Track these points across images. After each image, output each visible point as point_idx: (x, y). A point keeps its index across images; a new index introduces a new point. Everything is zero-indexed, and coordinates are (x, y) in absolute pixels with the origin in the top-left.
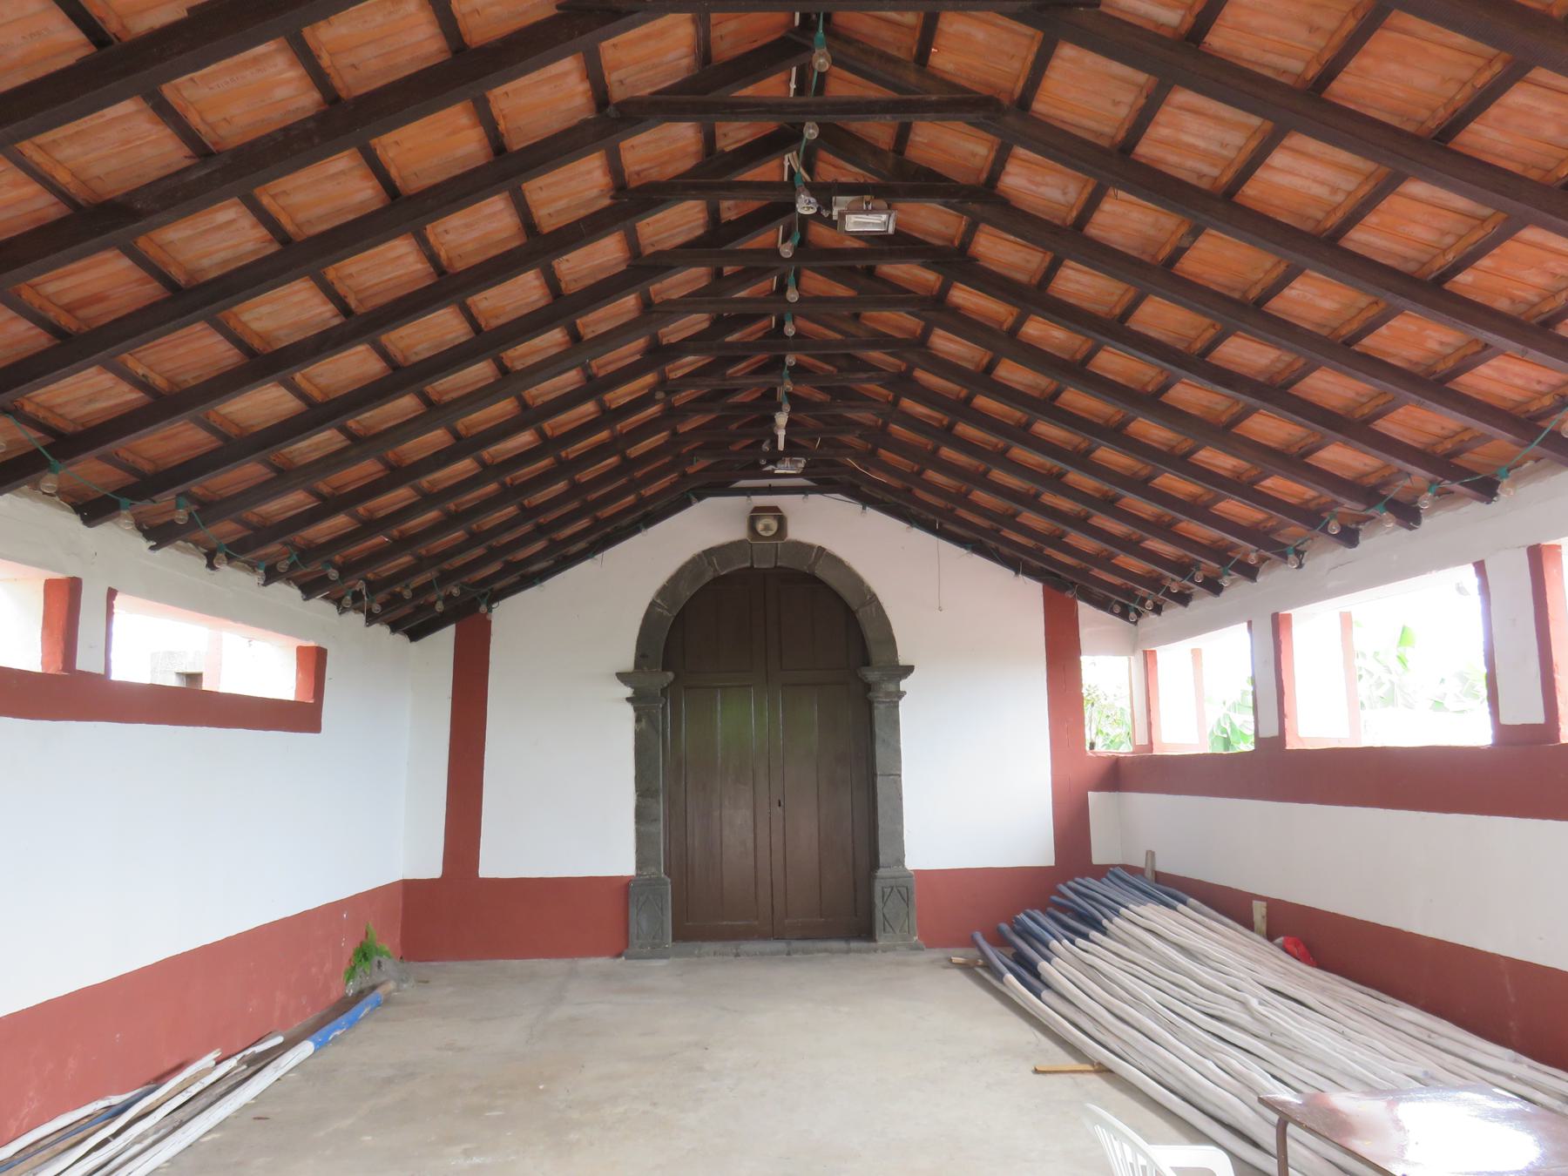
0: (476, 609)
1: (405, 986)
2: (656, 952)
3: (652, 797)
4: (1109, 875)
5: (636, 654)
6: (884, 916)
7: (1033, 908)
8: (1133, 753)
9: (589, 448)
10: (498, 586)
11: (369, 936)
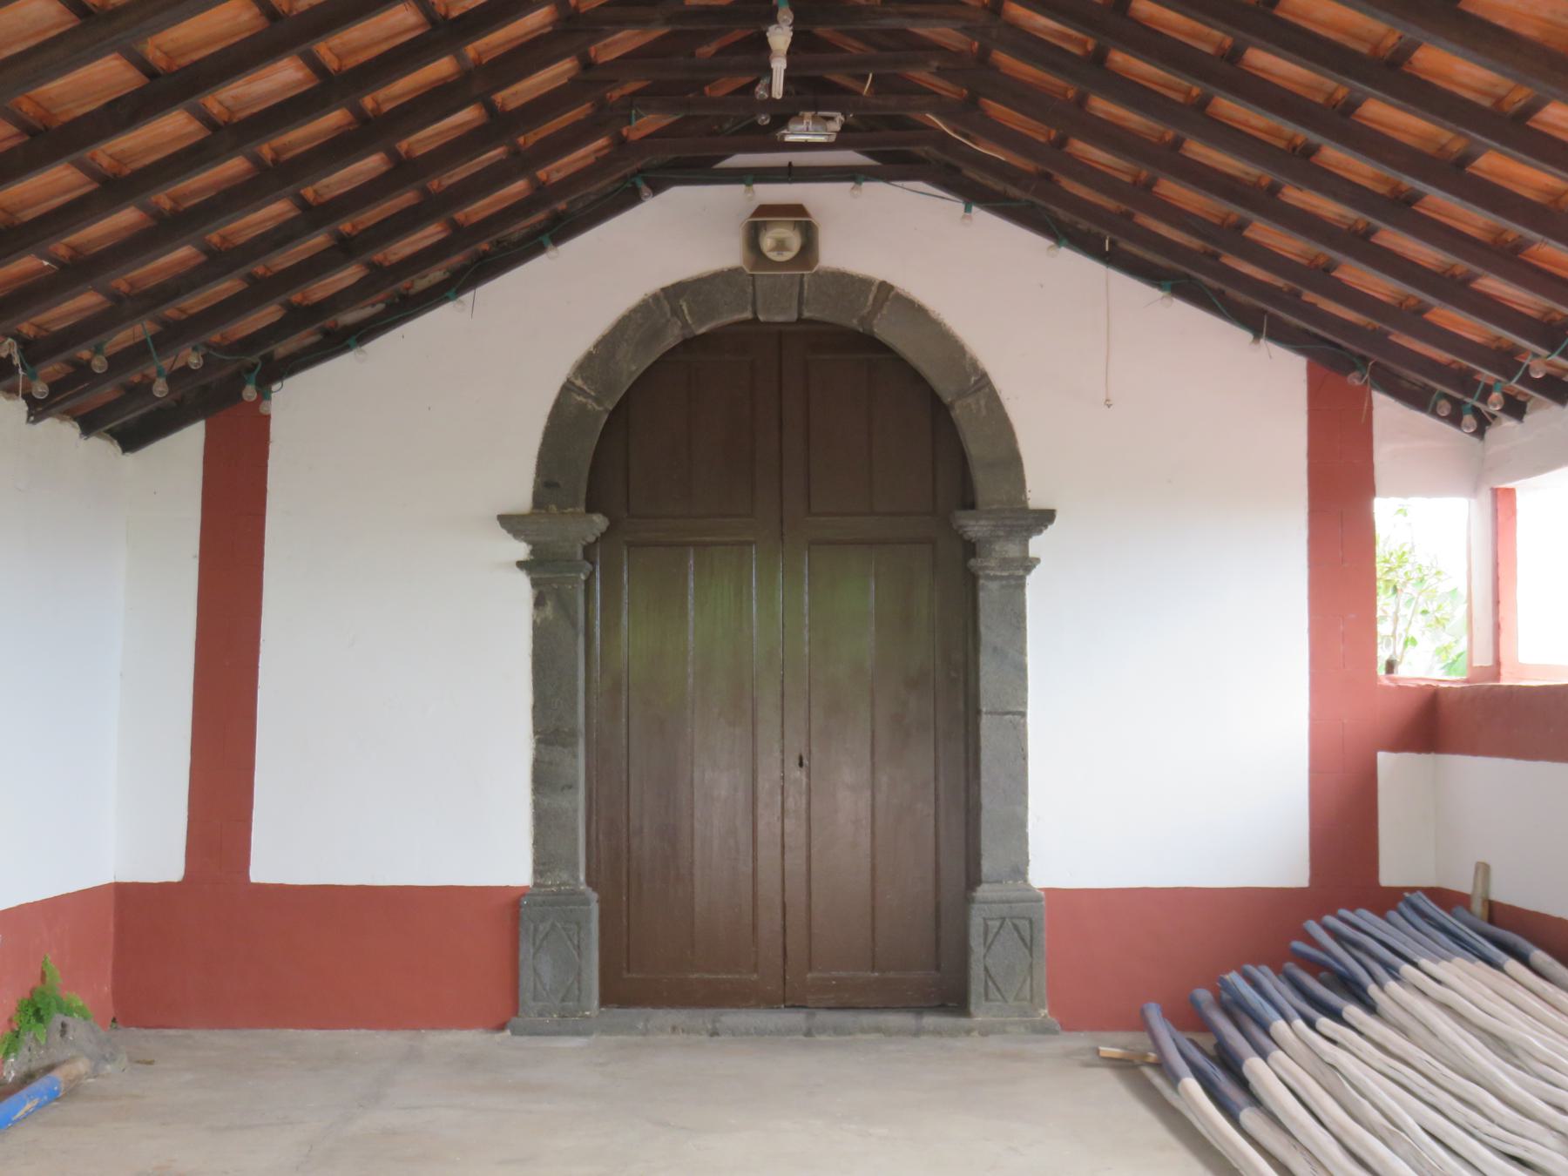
0: (237, 397)
1: (109, 1067)
2: (568, 1022)
3: (564, 746)
4: (1401, 905)
5: (535, 482)
6: (986, 969)
7: (1256, 964)
8: (1467, 681)
9: (414, 95)
10: (282, 349)
11: (48, 979)
